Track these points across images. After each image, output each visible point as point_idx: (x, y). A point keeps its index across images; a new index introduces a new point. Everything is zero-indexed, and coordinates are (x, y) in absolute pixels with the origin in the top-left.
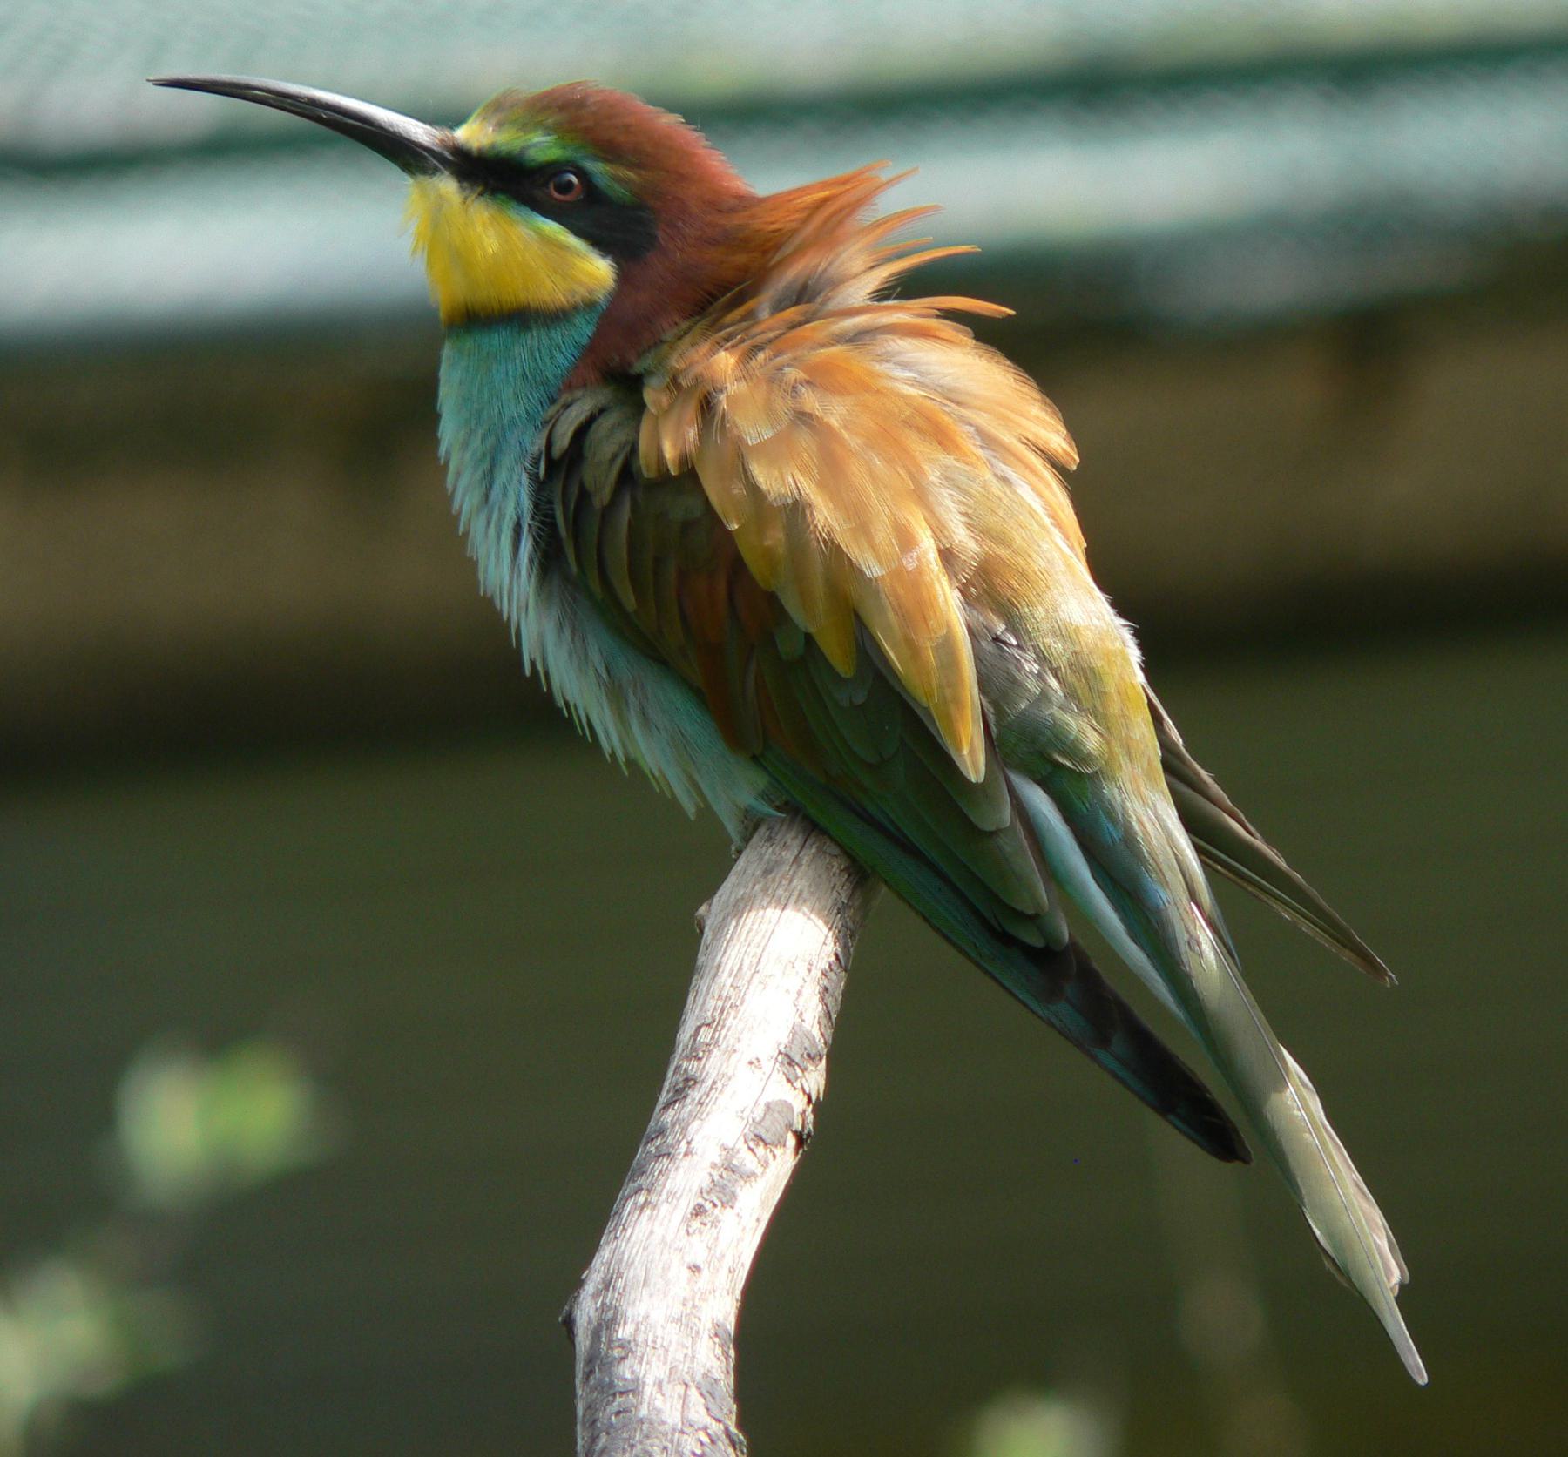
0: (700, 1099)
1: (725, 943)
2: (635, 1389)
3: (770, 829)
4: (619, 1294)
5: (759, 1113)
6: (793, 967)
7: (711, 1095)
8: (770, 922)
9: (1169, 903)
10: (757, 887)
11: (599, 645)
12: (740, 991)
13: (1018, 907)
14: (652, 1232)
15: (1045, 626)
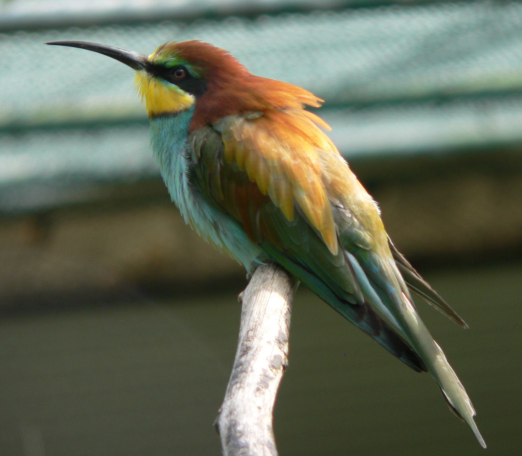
0: (253, 354)
1: (253, 305)
2: (247, 446)
3: (262, 268)
4: (236, 416)
5: (272, 358)
6: (276, 312)
7: (256, 353)
8: (267, 298)
9: (395, 292)
10: (261, 286)
11: (208, 211)
12: (261, 319)
13: (348, 291)
14: (244, 396)
15: (352, 202)
